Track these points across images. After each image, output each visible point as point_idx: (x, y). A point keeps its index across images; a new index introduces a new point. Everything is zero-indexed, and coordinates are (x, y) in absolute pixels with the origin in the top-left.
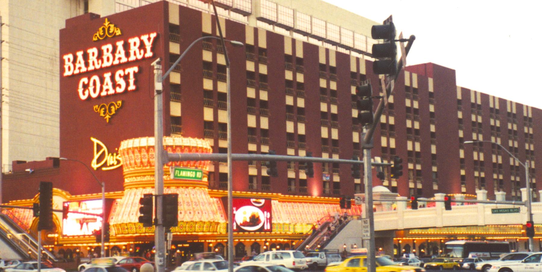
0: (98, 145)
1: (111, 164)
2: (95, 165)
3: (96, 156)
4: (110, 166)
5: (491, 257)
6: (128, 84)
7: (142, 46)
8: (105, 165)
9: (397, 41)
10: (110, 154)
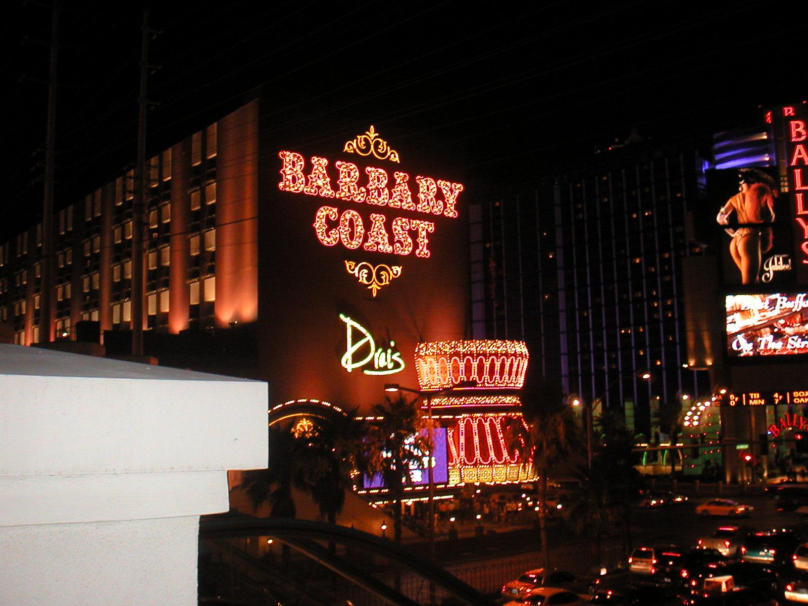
0: (354, 330)
1: (382, 366)
2: (348, 363)
3: (351, 349)
4: (380, 369)
5: (471, 322)
6: (416, 246)
7: (440, 196)
8: (370, 366)
9: (673, 469)
10: (380, 350)
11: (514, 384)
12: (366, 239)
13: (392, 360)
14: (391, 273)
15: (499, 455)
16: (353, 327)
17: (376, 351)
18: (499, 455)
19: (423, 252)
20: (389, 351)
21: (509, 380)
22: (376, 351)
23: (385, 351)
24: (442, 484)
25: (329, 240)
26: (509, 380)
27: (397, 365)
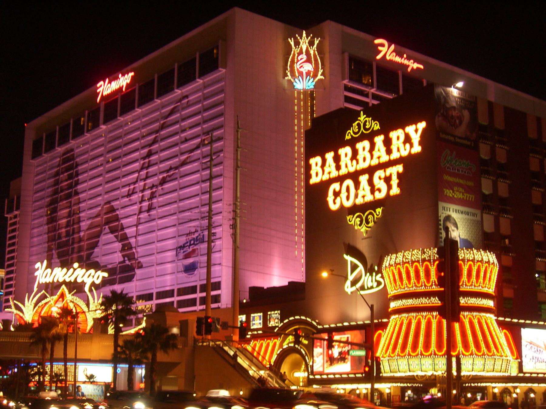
1: (369, 287)
3: (351, 277)
4: (368, 289)
7: (408, 139)
8: (362, 288)
10: (368, 274)
11: (482, 287)
12: (356, 196)
13: (376, 281)
14: (375, 214)
15: (427, 346)
16: (351, 262)
17: (366, 275)
18: (427, 346)
19: (395, 191)
20: (374, 274)
21: (484, 283)
22: (366, 275)
23: (371, 275)
24: (528, 373)
25: (334, 207)
26: (484, 283)
27: (379, 283)
